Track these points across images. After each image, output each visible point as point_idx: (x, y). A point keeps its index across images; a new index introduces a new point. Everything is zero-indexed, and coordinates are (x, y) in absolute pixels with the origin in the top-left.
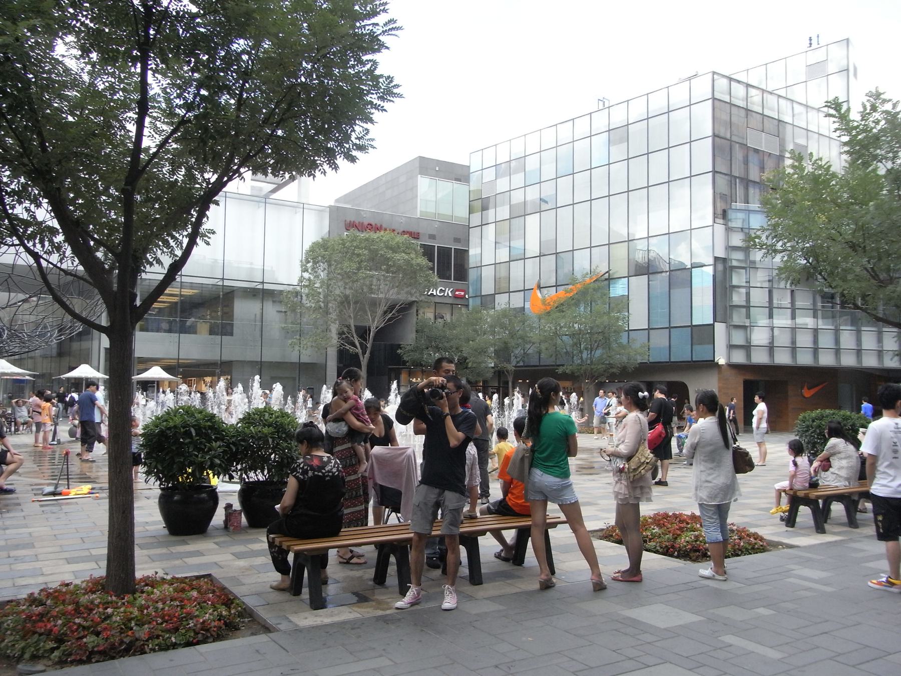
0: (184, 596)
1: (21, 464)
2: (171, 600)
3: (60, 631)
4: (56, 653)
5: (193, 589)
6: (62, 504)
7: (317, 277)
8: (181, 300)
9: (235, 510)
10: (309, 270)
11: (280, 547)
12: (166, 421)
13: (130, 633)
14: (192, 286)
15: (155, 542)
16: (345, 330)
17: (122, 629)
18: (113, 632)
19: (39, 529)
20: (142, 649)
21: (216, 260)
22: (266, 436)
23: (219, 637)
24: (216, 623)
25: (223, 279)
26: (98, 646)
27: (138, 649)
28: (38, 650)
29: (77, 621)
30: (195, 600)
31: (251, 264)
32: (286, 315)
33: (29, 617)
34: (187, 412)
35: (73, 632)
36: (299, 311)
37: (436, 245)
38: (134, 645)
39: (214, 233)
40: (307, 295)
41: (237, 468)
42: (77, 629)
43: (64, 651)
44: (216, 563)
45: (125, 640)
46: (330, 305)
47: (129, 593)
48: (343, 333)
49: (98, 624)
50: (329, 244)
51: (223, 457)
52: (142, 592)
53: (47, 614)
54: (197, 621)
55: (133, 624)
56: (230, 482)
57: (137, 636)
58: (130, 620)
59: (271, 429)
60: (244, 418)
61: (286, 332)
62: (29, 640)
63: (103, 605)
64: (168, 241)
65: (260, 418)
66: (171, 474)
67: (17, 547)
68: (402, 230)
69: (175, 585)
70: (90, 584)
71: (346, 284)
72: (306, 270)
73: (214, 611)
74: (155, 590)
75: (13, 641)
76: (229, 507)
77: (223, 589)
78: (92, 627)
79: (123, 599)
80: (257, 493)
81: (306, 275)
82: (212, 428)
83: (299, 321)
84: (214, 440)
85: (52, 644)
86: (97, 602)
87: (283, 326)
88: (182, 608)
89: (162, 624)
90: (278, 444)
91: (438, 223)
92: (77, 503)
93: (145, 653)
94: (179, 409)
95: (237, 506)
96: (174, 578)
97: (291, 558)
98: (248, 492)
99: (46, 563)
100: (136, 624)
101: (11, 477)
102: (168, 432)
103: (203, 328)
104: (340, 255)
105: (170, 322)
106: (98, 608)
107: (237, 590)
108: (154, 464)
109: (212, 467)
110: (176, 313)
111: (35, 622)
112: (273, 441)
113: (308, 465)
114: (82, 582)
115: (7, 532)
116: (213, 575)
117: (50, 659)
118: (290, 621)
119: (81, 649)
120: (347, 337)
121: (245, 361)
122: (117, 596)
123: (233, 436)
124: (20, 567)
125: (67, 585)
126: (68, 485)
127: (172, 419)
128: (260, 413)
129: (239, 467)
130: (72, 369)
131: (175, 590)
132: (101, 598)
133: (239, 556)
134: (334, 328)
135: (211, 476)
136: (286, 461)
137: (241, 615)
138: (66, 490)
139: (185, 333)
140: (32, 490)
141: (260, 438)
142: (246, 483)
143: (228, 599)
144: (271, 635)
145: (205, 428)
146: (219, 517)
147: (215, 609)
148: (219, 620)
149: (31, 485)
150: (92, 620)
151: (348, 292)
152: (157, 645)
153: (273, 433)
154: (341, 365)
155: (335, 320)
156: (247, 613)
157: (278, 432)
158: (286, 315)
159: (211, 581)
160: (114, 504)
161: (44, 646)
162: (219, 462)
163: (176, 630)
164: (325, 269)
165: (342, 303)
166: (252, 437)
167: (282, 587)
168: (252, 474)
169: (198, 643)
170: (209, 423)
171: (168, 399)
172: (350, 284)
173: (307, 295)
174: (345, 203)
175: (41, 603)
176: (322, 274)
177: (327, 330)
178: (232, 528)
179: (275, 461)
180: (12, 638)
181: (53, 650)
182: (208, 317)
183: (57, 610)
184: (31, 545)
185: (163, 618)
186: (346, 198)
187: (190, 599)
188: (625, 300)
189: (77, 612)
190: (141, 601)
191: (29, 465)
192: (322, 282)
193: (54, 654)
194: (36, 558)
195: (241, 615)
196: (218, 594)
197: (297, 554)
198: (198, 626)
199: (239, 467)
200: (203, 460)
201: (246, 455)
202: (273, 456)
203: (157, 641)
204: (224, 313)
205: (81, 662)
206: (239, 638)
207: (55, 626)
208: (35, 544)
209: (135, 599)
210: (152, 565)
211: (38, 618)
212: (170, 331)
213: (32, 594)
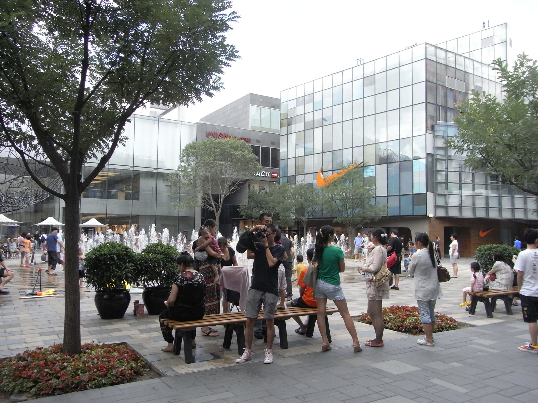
0: (110, 355)
1: (13, 277)
2: (102, 358)
3: (36, 376)
4: (34, 390)
5: (115, 351)
6: (37, 301)
7: (189, 165)
8: (108, 179)
9: (140, 304)
10: (185, 161)
11: (167, 326)
12: (99, 251)
13: (77, 377)
14: (115, 170)
15: (92, 323)
16: (206, 197)
17: (73, 375)
18: (68, 377)
19: (24, 315)
20: (85, 387)
21: (129, 155)
22: (159, 260)
23: (131, 380)
24: (129, 372)
25: (133, 166)
26: (58, 385)
27: (83, 387)
28: (23, 388)
29: (46, 370)
30: (116, 358)
31: (150, 157)
32: (171, 188)
33: (17, 368)
34: (112, 246)
35: (43, 377)
36: (178, 185)
37: (261, 146)
38: (80, 385)
39: (128, 139)
40: (183, 176)
41: (141, 279)
42: (46, 375)
43: (38, 388)
44: (129, 336)
45: (75, 381)
46: (197, 182)
47: (77, 354)
48: (205, 199)
49: (59, 372)
50: (197, 146)
51: (133, 273)
52: (85, 353)
53: (28, 366)
54: (118, 370)
55: (79, 372)
56: (137, 287)
57: (82, 379)
58: (78, 370)
59: (162, 256)
60: (146, 249)
61: (171, 198)
62: (17, 382)
63: (62, 361)
64: (100, 144)
65: (155, 249)
66: (102, 282)
67: (10, 326)
68: (240, 137)
69: (105, 349)
70: (54, 348)
71: (207, 169)
72: (183, 161)
73: (128, 364)
74: (93, 352)
75: (8, 382)
76: (137, 302)
77: (133, 351)
78: (55, 374)
79: (74, 357)
80: (153, 294)
81: (183, 164)
82: (126, 255)
83: (178, 192)
84: (128, 262)
85: (31, 384)
86: (58, 359)
87: (169, 194)
88: (108, 363)
89: (97, 372)
90: (166, 265)
91: (261, 133)
92: (46, 300)
93: (87, 389)
94: (107, 244)
95: (141, 301)
96: (104, 345)
97: (174, 332)
98: (148, 294)
99: (28, 335)
100: (81, 372)
101: (6, 285)
102: (100, 257)
103: (121, 195)
104: (203, 152)
105: (102, 192)
106: (59, 362)
107: (141, 352)
108: (92, 277)
109: (126, 278)
110: (105, 186)
111: (21, 371)
112: (163, 263)
114: (49, 347)
115: (4, 317)
116: (127, 343)
117: (30, 393)
118: (173, 370)
119: (48, 387)
120: (207, 201)
121: (146, 215)
122: (70, 355)
123: (139, 260)
124: (12, 338)
125: (40, 349)
126: (41, 289)
127: (103, 250)
128: (155, 246)
129: (143, 278)
130: (43, 220)
131: (105, 352)
132: (60, 357)
133: (142, 331)
134: (200, 196)
135: (126, 283)
136: (171, 275)
137: (144, 367)
138: (39, 292)
139: (111, 198)
140: (19, 292)
141: (155, 261)
142: (147, 288)
143: (136, 357)
144: (162, 378)
145: (122, 255)
146: (131, 308)
147: (129, 363)
148: (131, 370)
149: (19, 289)
150: (55, 370)
151: (208, 174)
152: (93, 385)
153: (163, 258)
154: (204, 218)
155: (200, 191)
156: (147, 366)
157: (166, 257)
158: (171, 188)
159: (126, 346)
161: (26, 385)
162: (131, 275)
163: (105, 375)
164: (194, 160)
165: (204, 181)
166: (151, 261)
167: (168, 350)
168: (150, 283)
169: (118, 383)
170: (125, 252)
171: (101, 238)
172: (209, 169)
173: (183, 176)
174: (206, 121)
175: (24, 360)
176: (192, 163)
177: (196, 197)
178: (138, 315)
179: (164, 275)
180: (7, 380)
181: (31, 387)
182: (124, 189)
183: (34, 363)
184: (19, 325)
185: (97, 368)
186: (207, 118)
187: (114, 357)
188: (373, 179)
189: (46, 365)
190: (84, 358)
191: (17, 277)
192: (192, 168)
193: (32, 390)
194: (22, 333)
195: (144, 367)
196: (130, 354)
197: (178, 331)
198: (119, 373)
199: (143, 278)
200: (121, 274)
201: (147, 271)
202: (163, 272)
203: (93, 382)
204: (134, 187)
205: (48, 395)
206: (143, 380)
207: (33, 373)
208: (21, 324)
209: (81, 357)
210: (91, 337)
211: (23, 368)
212: (101, 197)
213: (19, 354)
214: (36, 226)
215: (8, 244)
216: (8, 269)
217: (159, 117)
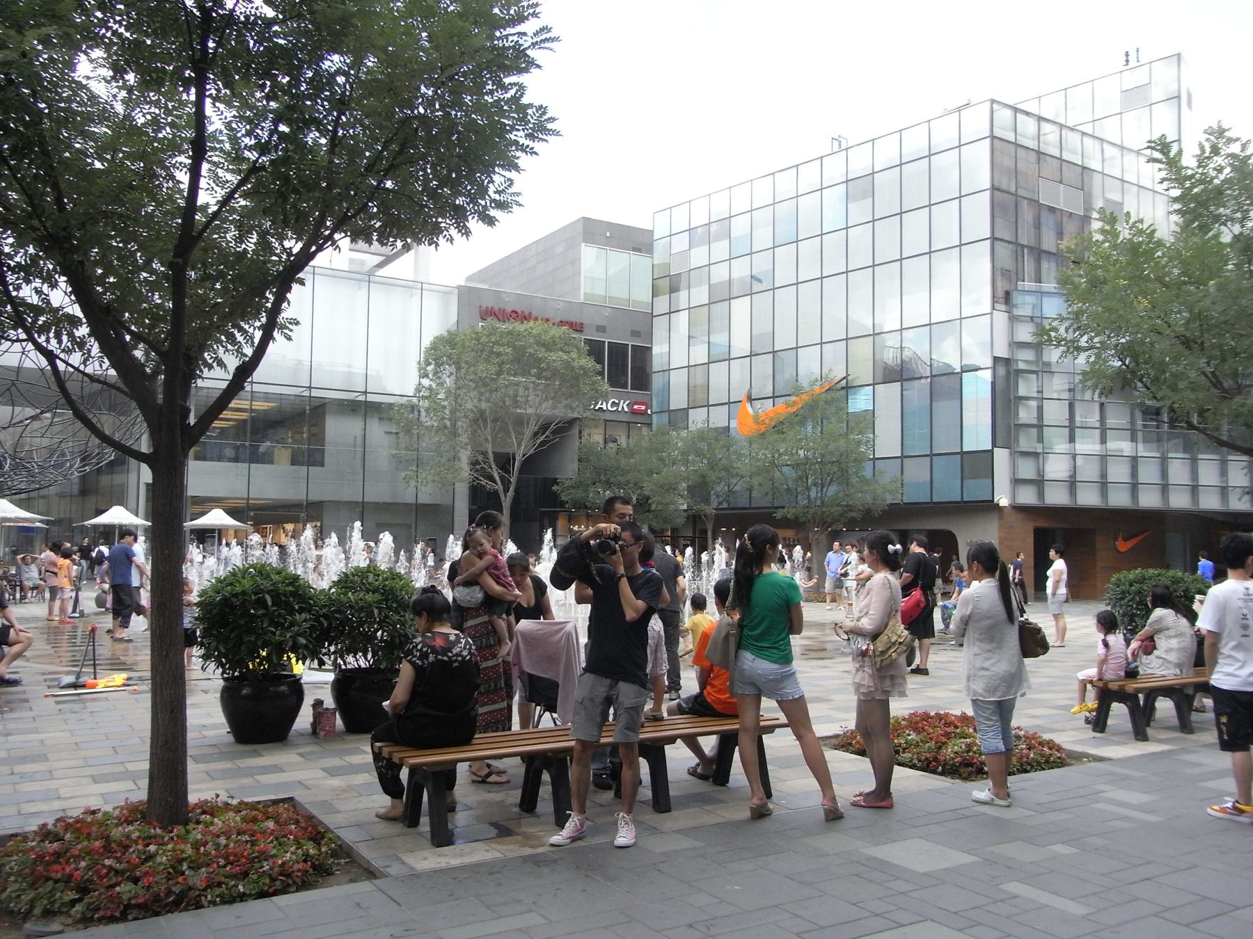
0: (256, 828)
1: (30, 645)
2: (238, 834)
3: (83, 877)
4: (78, 908)
5: (268, 818)
6: (87, 700)
7: (441, 384)
8: (252, 417)
9: (327, 709)
10: (430, 376)
11: (389, 760)
12: (231, 584)
13: (180, 879)
14: (267, 397)
15: (215, 752)
16: (480, 458)
17: (169, 873)
18: (157, 878)
19: (55, 735)
20: (198, 902)
21: (300, 362)
22: (371, 606)
23: (304, 885)
24: (300, 866)
25: (310, 388)
26: (136, 897)
27: (193, 902)
28: (53, 903)
29: (107, 862)
30: (271, 834)
31: (350, 366)
32: (398, 438)
33: (41, 857)
34: (260, 572)
35: (101, 878)
36: (416, 432)
37: (607, 341)
38: (187, 896)
39: (297, 323)
40: (427, 410)
41: (329, 650)
42: (107, 874)
43: (90, 904)
44: (300, 782)
45: (174, 889)
46: (459, 423)
47: (179, 824)
48: (477, 463)
49: (137, 866)
50: (458, 339)
51: (311, 635)
52: (198, 822)
53: (65, 853)
54: (274, 863)
55: (185, 867)
56: (320, 669)
57: (191, 883)
58: (181, 861)
59: (377, 596)
60: (339, 581)
61: (398, 461)
62: (41, 890)
63: (143, 840)
64: (233, 335)
65: (362, 580)
66: (237, 658)
67: (24, 760)
68: (559, 320)
69: (244, 813)
70: (125, 811)
71: (481, 394)
72: (425, 376)
73: (297, 849)
74: (216, 820)
75: (18, 890)
76: (318, 704)
77: (311, 818)
78: (128, 870)
79: (172, 832)
80: (357, 685)
81: (426, 382)
82: (294, 594)
83: (416, 446)
84: (297, 611)
85: (72, 895)
86: (135, 836)
87: (394, 452)
88: (253, 845)
89: (225, 866)
90: (386, 617)
91: (609, 309)
92: (107, 699)
93: (202, 907)
94: (248, 568)
95: (329, 702)
96: (241, 803)
97: (404, 774)
98: (345, 684)
99: (64, 781)
100: (189, 867)
101: (15, 663)
102: (234, 600)
103: (283, 455)
104: (473, 354)
105: (236, 448)
106: (137, 844)
107: (329, 820)
108: (214, 644)
109: (294, 649)
110: (245, 435)
111: (48, 864)
112: (380, 613)
113: (429, 647)
114: (115, 809)
115: (10, 738)
116: (297, 798)
117: (70, 916)
118: (404, 863)
119: (113, 902)
120: (482, 468)
121: (340, 502)
122: (163, 828)
123: (325, 606)
124: (28, 787)
125: (94, 812)
126: (95, 673)
127: (240, 582)
128: (361, 573)
129: (332, 649)
130: (100, 512)
131: (244, 820)
132: (140, 831)
133: (332, 772)
134: (465, 456)
135: (294, 661)
136: (397, 640)
137: (335, 854)
138: (91, 681)
139: (258, 462)
140: (45, 680)
141: (361, 609)
142: (341, 671)
143: (316, 832)
144: (377, 882)
145: (285, 595)
146: (304, 719)
147: (299, 846)
148: (305, 861)
149: (44, 674)
150: (128, 862)
151: (484, 405)
152: (218, 896)
153: (379, 602)
154: (475, 507)
155: (466, 444)
156: (343, 852)
157: (387, 600)
158: (398, 438)
159: (294, 806)
160: (158, 700)
161: (61, 898)
162: (304, 642)
163: (245, 874)
164: (451, 374)
165: (475, 421)
166: (351, 607)
167: (392, 815)
168: (350, 659)
169: (275, 893)
170: (291, 588)
172: (487, 395)
173: (427, 410)
174: (480, 282)
175: (57, 838)
176: (448, 380)
177: (455, 458)
178: (322, 733)
179: (382, 640)
180: (17, 886)
181: (73, 903)
182: (290, 440)
183: (79, 847)
184: (43, 758)
185: (226, 858)
186: (481, 275)
187: (265, 832)
188: (869, 417)
189: (107, 849)
190: (197, 835)
191: (40, 646)
192: (448, 392)
193: (75, 909)
194: (50, 775)
195: (335, 854)
196: (303, 825)
197: (414, 770)
198: (276, 869)
199: (332, 649)
200: (282, 639)
201: (342, 632)
202: (379, 633)
203: (218, 891)
204: (312, 435)
205: (112, 920)
206: (332, 886)
207: (77, 869)
208: (49, 755)
209: (188, 832)
210: (212, 785)
211: (53, 859)
212: (236, 460)
213: (45, 825)
216: (18, 626)
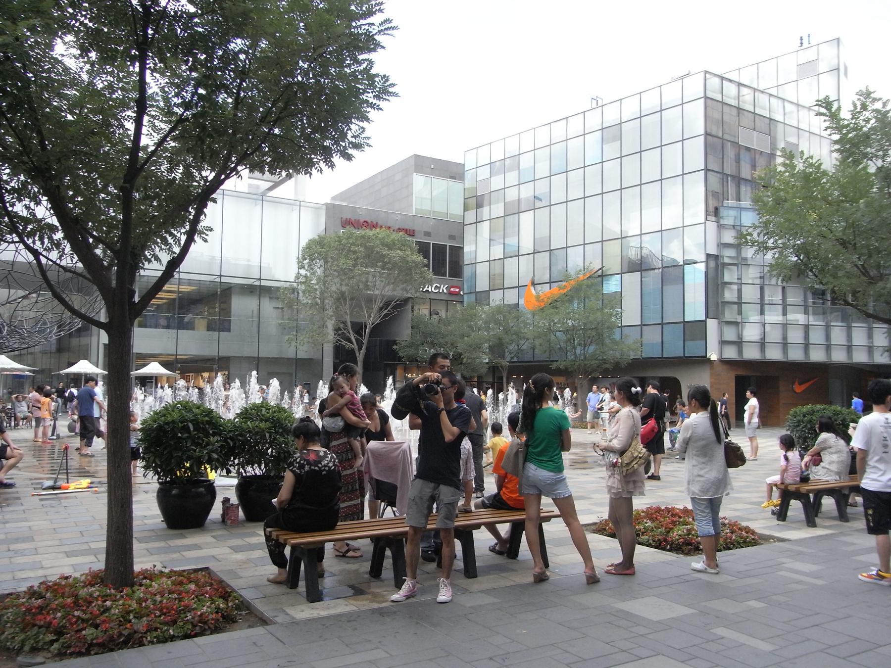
0: (182, 589)
1: (21, 459)
2: (170, 593)
3: (59, 624)
4: (56, 646)
5: (191, 582)
6: (62, 498)
7: (314, 273)
8: (179, 297)
9: (233, 504)
10: (306, 267)
11: (277, 541)
12: (164, 416)
13: (128, 625)
14: (190, 282)
15: (153, 535)
16: (342, 326)
17: (120, 621)
18: (112, 625)
19: (39, 523)
20: (141, 642)
21: (214, 257)
22: (263, 431)
23: (216, 630)
24: (214, 616)
25: (220, 276)
26: (97, 638)
27: (137, 642)
28: (37, 642)
29: (76, 613)
30: (193, 593)
31: (249, 261)
32: (283, 312)
33: (29, 610)
34: (185, 407)
35: (72, 624)
36: (295, 307)
37: (431, 242)
38: (133, 637)
39: (211, 230)
40: (304, 292)
41: (234, 463)
42: (76, 622)
43: (64, 643)
44: (213, 557)
45: (124, 632)
46: (327, 301)
47: (127, 586)
48: (339, 329)
49: (97, 616)
50: (326, 241)
51: (221, 452)
52: (141, 585)
53: (47, 607)
54: (195, 614)
55: (131, 617)
56: (227, 476)
57: (136, 628)
58: (128, 613)
59: (268, 424)
60: (241, 413)
61: (283, 328)
62: (29, 633)
63: (102, 598)
64: (166, 239)
65: (257, 413)
66: (169, 468)
67: (17, 540)
68: (397, 227)
69: (173, 578)
70: (89, 577)
71: (342, 280)
72: (303, 267)
73: (211, 604)
74: (153, 583)
75: (13, 633)
76: (226, 501)
77: (221, 582)
78: (91, 619)
79: (122, 592)
80: (254, 487)
81: (303, 272)
82: (209, 423)
83: (296, 318)
84: (211, 435)
85: (51, 637)
86: (96, 594)
87: (280, 322)
88: (180, 601)
89: (160, 616)
90: (275, 439)
91: (433, 220)
92: (76, 497)
93: (144, 645)
94: (177, 404)
95: (234, 500)
96: (172, 571)
97: (287, 551)
98: (245, 487)
99: (46, 556)
100: (135, 617)
101: (11, 472)
102: (166, 427)
103: (201, 324)
104: (336, 252)
105: (168, 319)
106: (97, 601)
107: (234, 583)
108: (152, 458)
109: (209, 462)
110: (174, 309)
111: (34, 614)
112: (270, 436)
114: (82, 575)
115: (7, 525)
116: (211, 568)
117: (50, 652)
118: (287, 614)
119: (80, 642)
120: (343, 333)
121: (242, 357)
122: (116, 589)
123: (231, 431)
124: (20, 560)
125: (67, 578)
126: (67, 479)
127: (170, 414)
128: (257, 408)
129: (236, 461)
130: (71, 364)
131: (173, 583)
132: (100, 591)
133: (236, 549)
134: (330, 324)
135: (209, 470)
136: (282, 456)
137: (238, 608)
138: (65, 485)
139: (183, 329)
140: (32, 484)
141: (257, 433)
142: (243, 477)
143: (225, 592)
144: (268, 627)
145: (202, 423)
146: (216, 511)
147: (213, 602)
148: (217, 613)
149: (31, 479)
150: (91, 613)
151: (344, 288)
152: (155, 637)
153: (270, 428)
155: (332, 316)
156: (244, 606)
157: (275, 427)
158: (283, 312)
159: (209, 574)
160: (113, 498)
161: (43, 639)
162: (216, 457)
163: (174, 622)
164: (321, 266)
165: (338, 299)
166: (250, 432)
167: (278, 580)
168: (249, 469)
169: (196, 635)
170: (207, 418)
171: (167, 394)
172: (346, 281)
173: (304, 292)
174: (341, 201)
175: (41, 596)
176: (318, 270)
177: (324, 326)
178: (229, 522)
179: (271, 456)
180: (12, 630)
181: (52, 642)
182: (206, 313)
183: (56, 602)
184: (31, 539)
185: (161, 611)
186: (342, 196)
187: (188, 592)
188: (618, 297)
189: (76, 604)
190: (140, 594)
191: (29, 459)
192: (319, 279)
193: (53, 647)
194: (36, 551)
195: (238, 608)
196: (215, 587)
197: (294, 548)
198: (196, 619)
199: (236, 461)
200: (201, 454)
201: (243, 450)
202: (270, 451)
203: (155, 634)
204: (222, 310)
205: (80, 654)
206: (236, 630)
207: (55, 618)
208: (35, 537)
209: (134, 592)
210: (151, 558)
211: (37, 611)
212: (168, 327)
213: (32, 587)
214: (59, 374)
215: (13, 404)
216: (13, 445)
217: (263, 195)
